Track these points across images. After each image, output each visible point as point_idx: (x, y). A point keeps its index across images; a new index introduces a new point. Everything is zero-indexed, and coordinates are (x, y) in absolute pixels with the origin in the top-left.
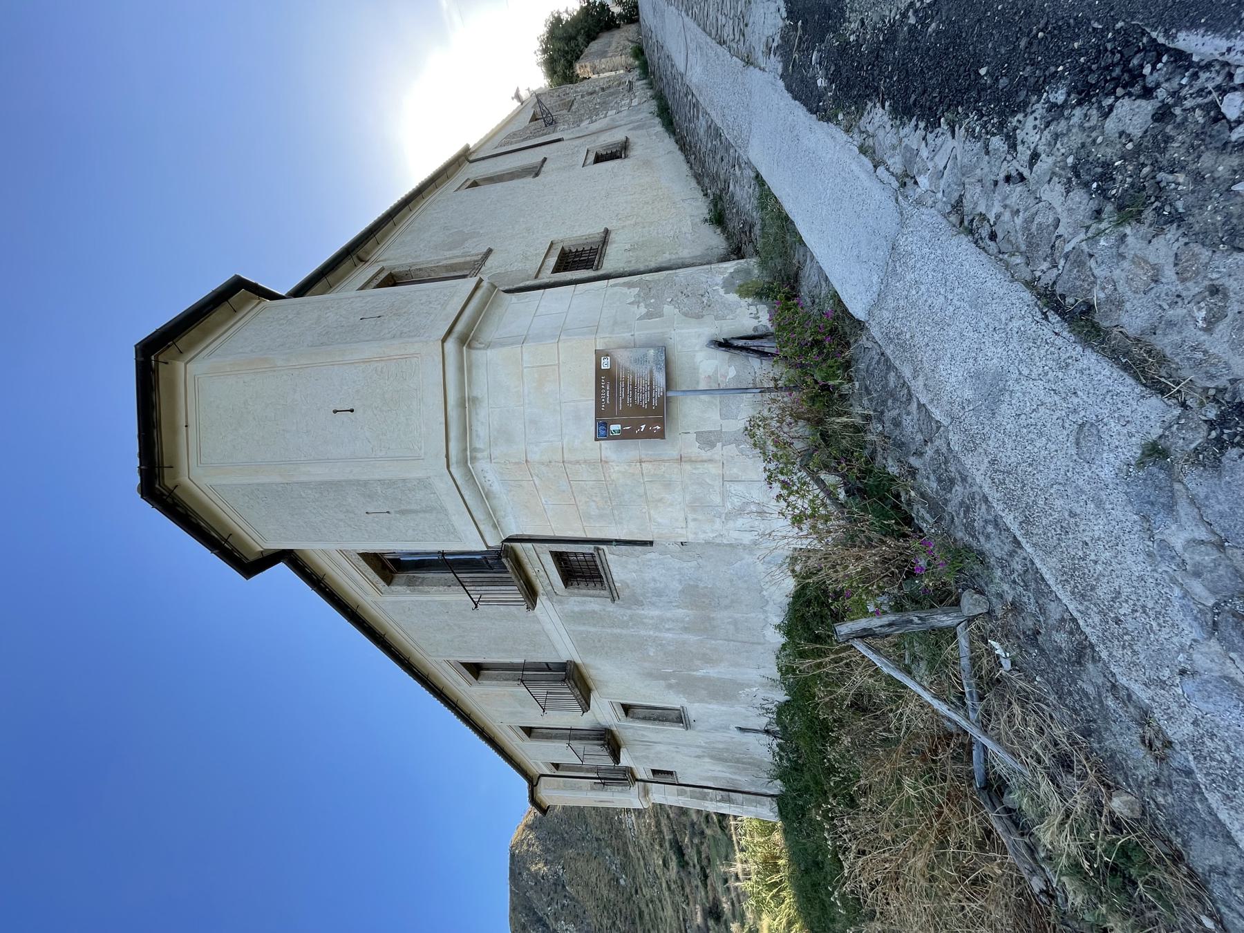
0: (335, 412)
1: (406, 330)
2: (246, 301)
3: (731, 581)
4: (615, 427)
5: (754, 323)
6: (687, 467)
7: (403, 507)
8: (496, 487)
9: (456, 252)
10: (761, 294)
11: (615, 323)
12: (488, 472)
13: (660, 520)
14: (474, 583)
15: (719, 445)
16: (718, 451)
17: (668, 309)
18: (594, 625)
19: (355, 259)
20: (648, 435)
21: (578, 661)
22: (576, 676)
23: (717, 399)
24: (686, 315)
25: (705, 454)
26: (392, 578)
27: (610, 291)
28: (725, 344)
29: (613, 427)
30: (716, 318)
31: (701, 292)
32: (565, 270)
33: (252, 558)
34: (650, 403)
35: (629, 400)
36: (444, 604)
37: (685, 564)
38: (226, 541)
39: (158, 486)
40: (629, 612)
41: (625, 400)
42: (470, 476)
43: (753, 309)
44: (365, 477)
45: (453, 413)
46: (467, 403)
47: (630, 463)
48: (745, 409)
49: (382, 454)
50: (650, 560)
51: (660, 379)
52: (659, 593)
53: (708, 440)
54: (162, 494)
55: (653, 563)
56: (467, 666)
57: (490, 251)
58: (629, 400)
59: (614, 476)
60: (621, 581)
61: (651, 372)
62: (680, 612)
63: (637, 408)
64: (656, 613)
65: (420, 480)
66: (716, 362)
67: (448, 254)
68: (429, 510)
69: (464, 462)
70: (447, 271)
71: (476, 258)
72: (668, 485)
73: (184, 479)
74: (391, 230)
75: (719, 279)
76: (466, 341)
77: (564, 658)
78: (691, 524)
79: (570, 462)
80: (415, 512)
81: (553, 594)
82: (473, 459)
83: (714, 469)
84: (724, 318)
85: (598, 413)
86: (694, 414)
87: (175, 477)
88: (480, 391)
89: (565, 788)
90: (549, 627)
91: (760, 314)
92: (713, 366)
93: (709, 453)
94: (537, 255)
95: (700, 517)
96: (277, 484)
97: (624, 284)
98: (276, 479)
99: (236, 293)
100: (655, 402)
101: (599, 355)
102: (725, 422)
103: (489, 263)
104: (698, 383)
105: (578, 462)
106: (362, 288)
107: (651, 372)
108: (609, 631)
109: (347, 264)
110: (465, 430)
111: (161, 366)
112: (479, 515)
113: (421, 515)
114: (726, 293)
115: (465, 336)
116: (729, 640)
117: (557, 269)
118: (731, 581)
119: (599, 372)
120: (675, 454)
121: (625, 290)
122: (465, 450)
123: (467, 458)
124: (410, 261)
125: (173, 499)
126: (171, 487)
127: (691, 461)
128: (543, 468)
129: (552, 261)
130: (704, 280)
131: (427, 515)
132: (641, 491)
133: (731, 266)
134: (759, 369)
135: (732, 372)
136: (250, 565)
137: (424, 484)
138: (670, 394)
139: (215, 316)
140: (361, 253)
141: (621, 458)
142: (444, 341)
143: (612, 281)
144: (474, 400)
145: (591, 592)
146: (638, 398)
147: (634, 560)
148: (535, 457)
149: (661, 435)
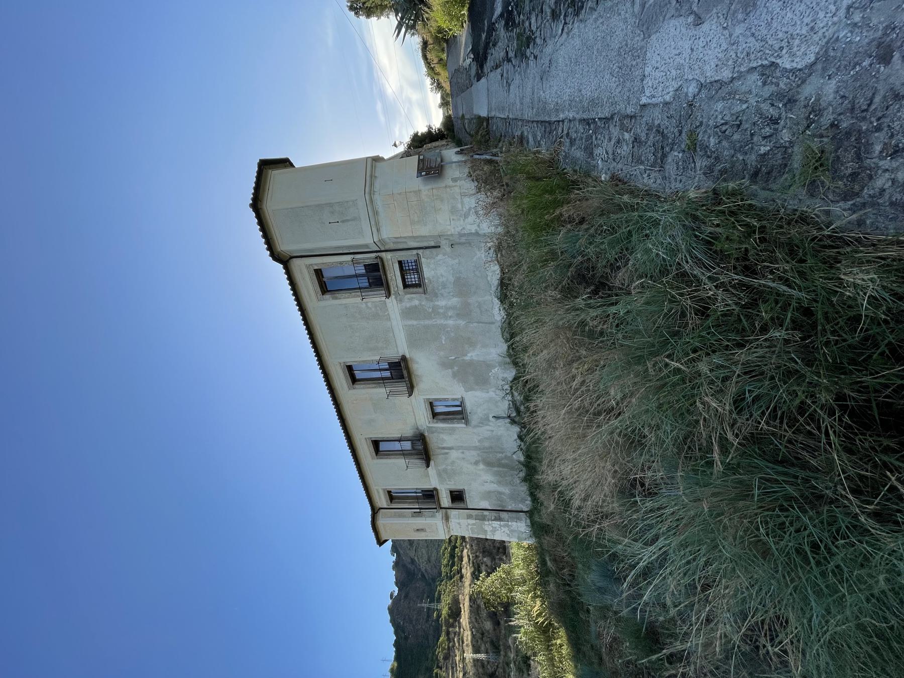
16: (459, 183)
25: (454, 184)
39: (257, 204)
45: (368, 179)
53: (455, 180)
63: (431, 168)
80: (348, 221)
89: (395, 516)
110: (371, 185)
144: (376, 177)
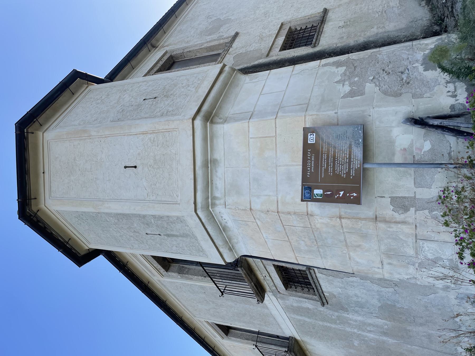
0: (126, 167)
1: (170, 109)
2: (79, 87)
3: (426, 307)
4: (317, 192)
5: (452, 101)
6: (382, 226)
7: (168, 233)
8: (230, 224)
9: (214, 36)
10: (458, 72)
11: (323, 101)
12: (224, 214)
13: (358, 260)
14: (221, 277)
15: (412, 210)
17: (369, 87)
18: (309, 318)
19: (149, 46)
20: (345, 200)
21: (298, 338)
22: (296, 349)
23: (411, 170)
24: (385, 93)
25: (399, 217)
26: (170, 266)
27: (322, 70)
28: (419, 122)
29: (316, 192)
30: (414, 96)
31: (401, 69)
32: (291, 47)
33: (82, 253)
34: (348, 174)
35: (330, 170)
36: (202, 287)
37: (383, 289)
38: (67, 243)
40: (336, 314)
41: (327, 170)
42: (211, 217)
43: (451, 87)
44: (144, 213)
45: (199, 172)
46: (209, 164)
47: (331, 218)
48: (438, 181)
49: (154, 197)
50: (353, 282)
51: (358, 153)
52: (361, 305)
54: (31, 215)
55: (355, 284)
56: (220, 326)
57: (237, 34)
58: (330, 170)
59: (318, 226)
60: (329, 292)
61: (350, 147)
62: (380, 322)
63: (337, 177)
64: (360, 318)
65: (178, 218)
66: (411, 137)
67: (209, 38)
68: (185, 236)
69: (206, 207)
70: (208, 51)
71: (227, 41)
72: (365, 236)
73: (42, 206)
74: (173, 22)
75: (420, 56)
76: (210, 118)
77: (287, 333)
78: (386, 267)
79: (283, 213)
81: (276, 292)
82: (214, 205)
83: (407, 229)
84: (421, 96)
85: (304, 179)
86: (388, 182)
87: (37, 204)
88: (219, 155)
90: (274, 312)
91: (459, 91)
92: (407, 140)
93: (402, 216)
94: (270, 35)
95: (395, 262)
96: (93, 213)
97: (334, 64)
98: (90, 209)
99: (76, 81)
100: (353, 173)
101: (306, 131)
102: (419, 190)
103: (235, 45)
104: (394, 154)
105: (289, 213)
106: (145, 75)
107: (350, 147)
108: (321, 323)
109: (145, 50)
110: (208, 184)
111: (30, 135)
112: (219, 242)
113: (180, 238)
114: (425, 70)
115: (209, 114)
116: (423, 347)
117: (284, 47)
118: (426, 307)
119: (306, 145)
120: (371, 214)
121: (334, 69)
122: (208, 198)
123: (209, 204)
124: (184, 45)
125: (37, 218)
126: (35, 211)
127: (385, 221)
128: (263, 215)
129: (281, 40)
130: (405, 56)
131: (184, 239)
132: (342, 238)
133: (432, 42)
134: (455, 146)
135: (427, 146)
136: (81, 257)
137: (180, 220)
138: (366, 166)
139: (62, 99)
140: (153, 41)
141: (324, 215)
142: (194, 119)
143: (324, 61)
145: (305, 295)
146: (338, 169)
147: (339, 280)
148: (257, 206)
149: (357, 201)
